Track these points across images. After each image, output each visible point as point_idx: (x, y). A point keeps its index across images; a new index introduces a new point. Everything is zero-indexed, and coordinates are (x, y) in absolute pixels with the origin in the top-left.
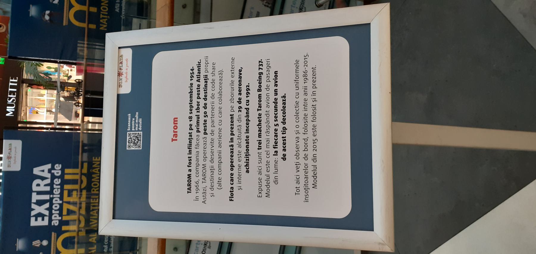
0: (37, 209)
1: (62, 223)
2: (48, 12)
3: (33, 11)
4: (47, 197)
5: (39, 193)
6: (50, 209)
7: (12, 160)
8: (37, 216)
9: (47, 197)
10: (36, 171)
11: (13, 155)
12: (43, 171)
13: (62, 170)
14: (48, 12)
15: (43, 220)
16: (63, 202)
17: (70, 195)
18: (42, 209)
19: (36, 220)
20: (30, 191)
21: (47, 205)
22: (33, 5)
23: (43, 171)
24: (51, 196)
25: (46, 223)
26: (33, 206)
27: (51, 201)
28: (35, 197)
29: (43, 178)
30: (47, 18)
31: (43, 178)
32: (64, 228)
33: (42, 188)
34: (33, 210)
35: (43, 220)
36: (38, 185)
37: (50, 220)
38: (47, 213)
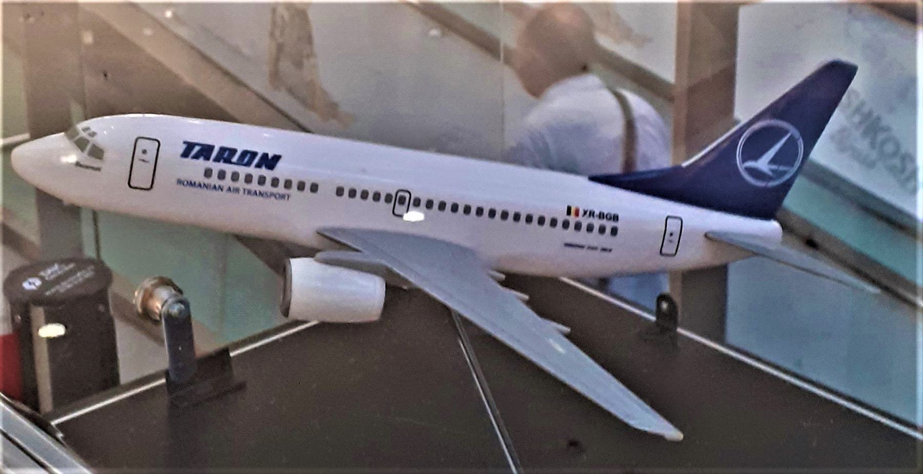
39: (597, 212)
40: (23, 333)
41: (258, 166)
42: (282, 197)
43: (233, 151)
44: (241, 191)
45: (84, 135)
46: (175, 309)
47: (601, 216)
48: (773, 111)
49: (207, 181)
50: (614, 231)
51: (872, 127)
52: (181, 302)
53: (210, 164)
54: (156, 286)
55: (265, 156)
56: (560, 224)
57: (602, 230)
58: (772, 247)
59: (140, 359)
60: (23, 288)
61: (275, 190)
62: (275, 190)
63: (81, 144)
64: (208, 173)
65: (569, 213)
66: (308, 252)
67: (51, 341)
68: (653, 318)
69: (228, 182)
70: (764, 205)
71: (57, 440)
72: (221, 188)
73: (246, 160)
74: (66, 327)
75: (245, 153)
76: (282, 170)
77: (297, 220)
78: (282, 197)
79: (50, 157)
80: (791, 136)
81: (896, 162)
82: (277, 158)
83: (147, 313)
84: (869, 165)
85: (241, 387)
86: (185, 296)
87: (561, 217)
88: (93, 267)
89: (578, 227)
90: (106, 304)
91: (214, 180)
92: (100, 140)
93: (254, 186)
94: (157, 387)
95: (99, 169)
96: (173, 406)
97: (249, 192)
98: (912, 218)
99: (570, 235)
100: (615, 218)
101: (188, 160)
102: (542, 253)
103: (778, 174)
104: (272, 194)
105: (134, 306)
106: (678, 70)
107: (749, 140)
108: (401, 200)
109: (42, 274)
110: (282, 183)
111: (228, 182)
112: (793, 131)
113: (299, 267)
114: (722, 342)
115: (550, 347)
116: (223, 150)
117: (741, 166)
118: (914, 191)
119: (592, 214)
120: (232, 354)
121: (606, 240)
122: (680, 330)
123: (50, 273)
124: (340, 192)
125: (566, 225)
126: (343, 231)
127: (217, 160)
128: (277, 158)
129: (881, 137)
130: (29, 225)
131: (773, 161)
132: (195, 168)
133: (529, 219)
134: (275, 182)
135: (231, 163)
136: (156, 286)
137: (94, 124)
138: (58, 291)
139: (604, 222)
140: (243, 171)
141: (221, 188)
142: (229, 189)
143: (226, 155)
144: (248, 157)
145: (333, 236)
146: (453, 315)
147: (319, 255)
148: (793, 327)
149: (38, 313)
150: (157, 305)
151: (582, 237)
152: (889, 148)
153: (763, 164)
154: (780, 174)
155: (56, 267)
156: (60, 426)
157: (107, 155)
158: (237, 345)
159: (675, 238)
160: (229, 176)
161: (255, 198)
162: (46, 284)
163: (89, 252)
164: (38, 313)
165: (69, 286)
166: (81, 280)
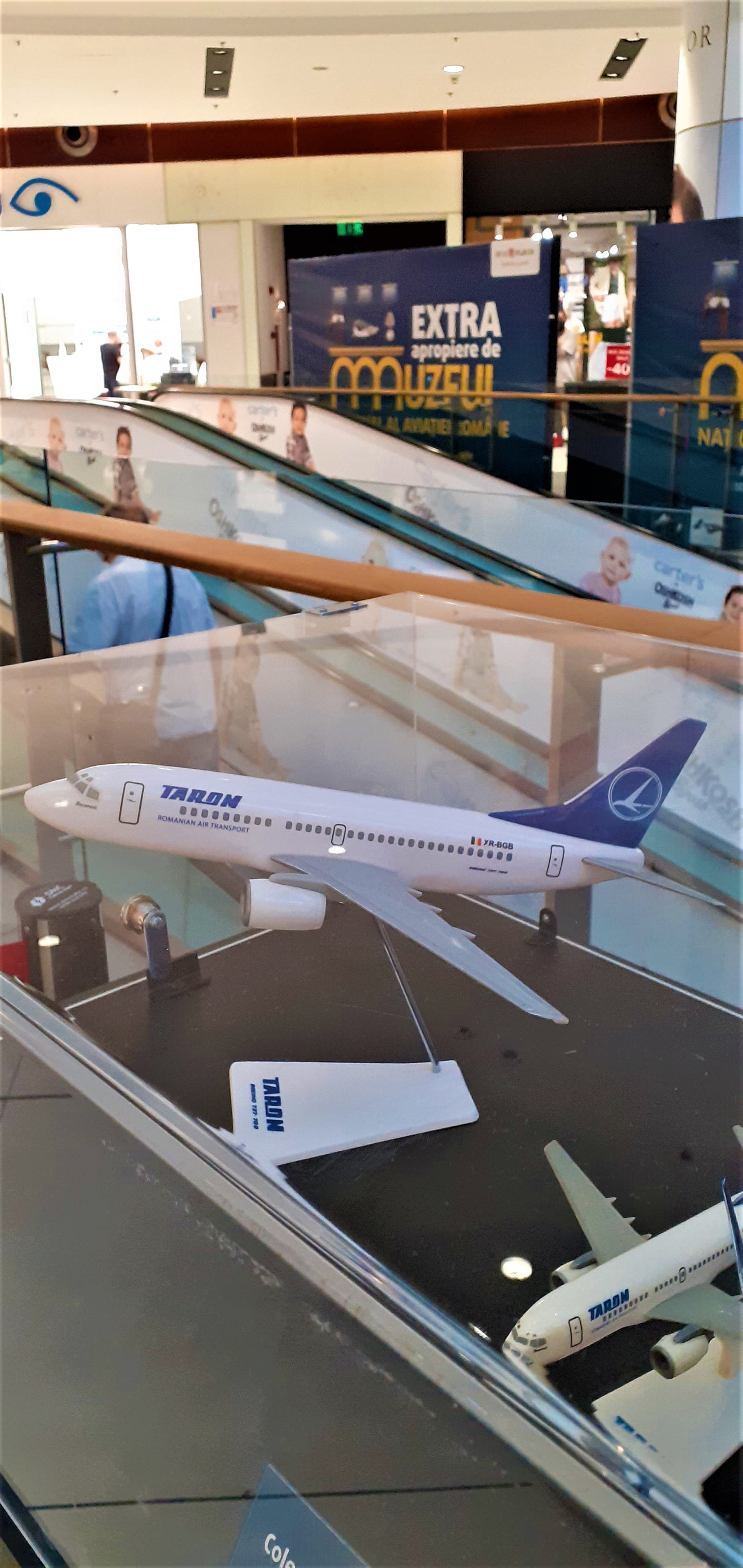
0: (435, 314)
1: (415, 363)
2: (726, 302)
3: (725, 268)
4: (452, 333)
5: (458, 316)
6: (435, 341)
7: (508, 259)
8: (425, 316)
9: (452, 333)
10: (491, 308)
11: (517, 259)
12: (490, 321)
13: (490, 360)
14: (726, 302)
15: (421, 328)
16: (444, 364)
17: (456, 378)
18: (435, 327)
19: (421, 316)
20: (460, 300)
21: (440, 335)
22: (738, 267)
23: (490, 321)
24: (453, 341)
25: (417, 334)
26: (440, 307)
27: (445, 341)
28: (451, 309)
29: (479, 322)
30: (714, 302)
31: (479, 322)
32: (408, 368)
33: (465, 322)
34: (435, 308)
35: (421, 328)
36: (469, 314)
37: (420, 342)
38: (429, 335)
39: (496, 843)
40: (31, 940)
41: (223, 805)
42: (243, 830)
43: (203, 793)
44: (210, 825)
45: (83, 780)
46: (154, 921)
47: (499, 845)
48: (635, 761)
49: (182, 817)
50: (509, 857)
51: (706, 776)
52: (157, 915)
53: (185, 803)
54: (139, 902)
55: (229, 796)
56: (466, 851)
57: (500, 856)
58: (635, 869)
59: (124, 963)
60: (31, 905)
61: (236, 824)
62: (236, 824)
63: (81, 787)
64: (183, 811)
65: (473, 843)
66: (264, 874)
67: (53, 948)
68: (537, 928)
69: (199, 818)
70: (628, 835)
71: (70, 1022)
72: (193, 823)
73: (213, 801)
74: (60, 938)
75: (212, 795)
76: (242, 809)
77: (255, 848)
78: (243, 830)
79: (54, 800)
80: (653, 780)
81: (724, 804)
82: (238, 798)
83: (132, 925)
84: (703, 807)
85: (207, 983)
86: (162, 911)
87: (467, 846)
88: (86, 888)
89: (480, 854)
90: (98, 919)
91: (188, 816)
92: (96, 784)
93: (220, 821)
94: (139, 984)
95: (95, 808)
96: (152, 998)
97: (216, 826)
98: (738, 850)
99: (474, 860)
100: (510, 846)
101: (167, 800)
102: (453, 874)
103: (643, 811)
104: (234, 828)
105: (122, 918)
106: (553, 733)
107: (619, 782)
108: (336, 833)
109: (46, 893)
110: (242, 819)
111: (199, 818)
112: (654, 776)
113: (258, 888)
114: (587, 945)
115: (456, 947)
116: (195, 792)
117: (612, 805)
118: (737, 829)
119: (492, 843)
120: (200, 957)
121: (503, 864)
122: (558, 937)
123: (52, 893)
124: (289, 826)
125: (470, 852)
126: (291, 857)
127: (190, 800)
128: (238, 798)
129: (712, 784)
130: (29, 854)
131: (636, 801)
132: (173, 806)
133: (441, 848)
134: (237, 818)
135: (200, 802)
136: (139, 902)
137: (91, 771)
138: (57, 908)
139: (501, 850)
140: (211, 809)
141: (193, 823)
142: (200, 824)
143: (198, 796)
144: (215, 798)
145: (283, 861)
146: (382, 927)
147: (272, 876)
148: (644, 930)
149: (43, 925)
150: (140, 918)
151: (483, 862)
152: (718, 793)
153: (629, 802)
154: (644, 810)
155: (57, 888)
156: (72, 1010)
157: (103, 797)
158: (204, 950)
159: (558, 862)
160: (199, 813)
161: (171, 823)
162: (50, 902)
163: (80, 877)
164: (43, 925)
165: (68, 903)
166: (77, 898)
